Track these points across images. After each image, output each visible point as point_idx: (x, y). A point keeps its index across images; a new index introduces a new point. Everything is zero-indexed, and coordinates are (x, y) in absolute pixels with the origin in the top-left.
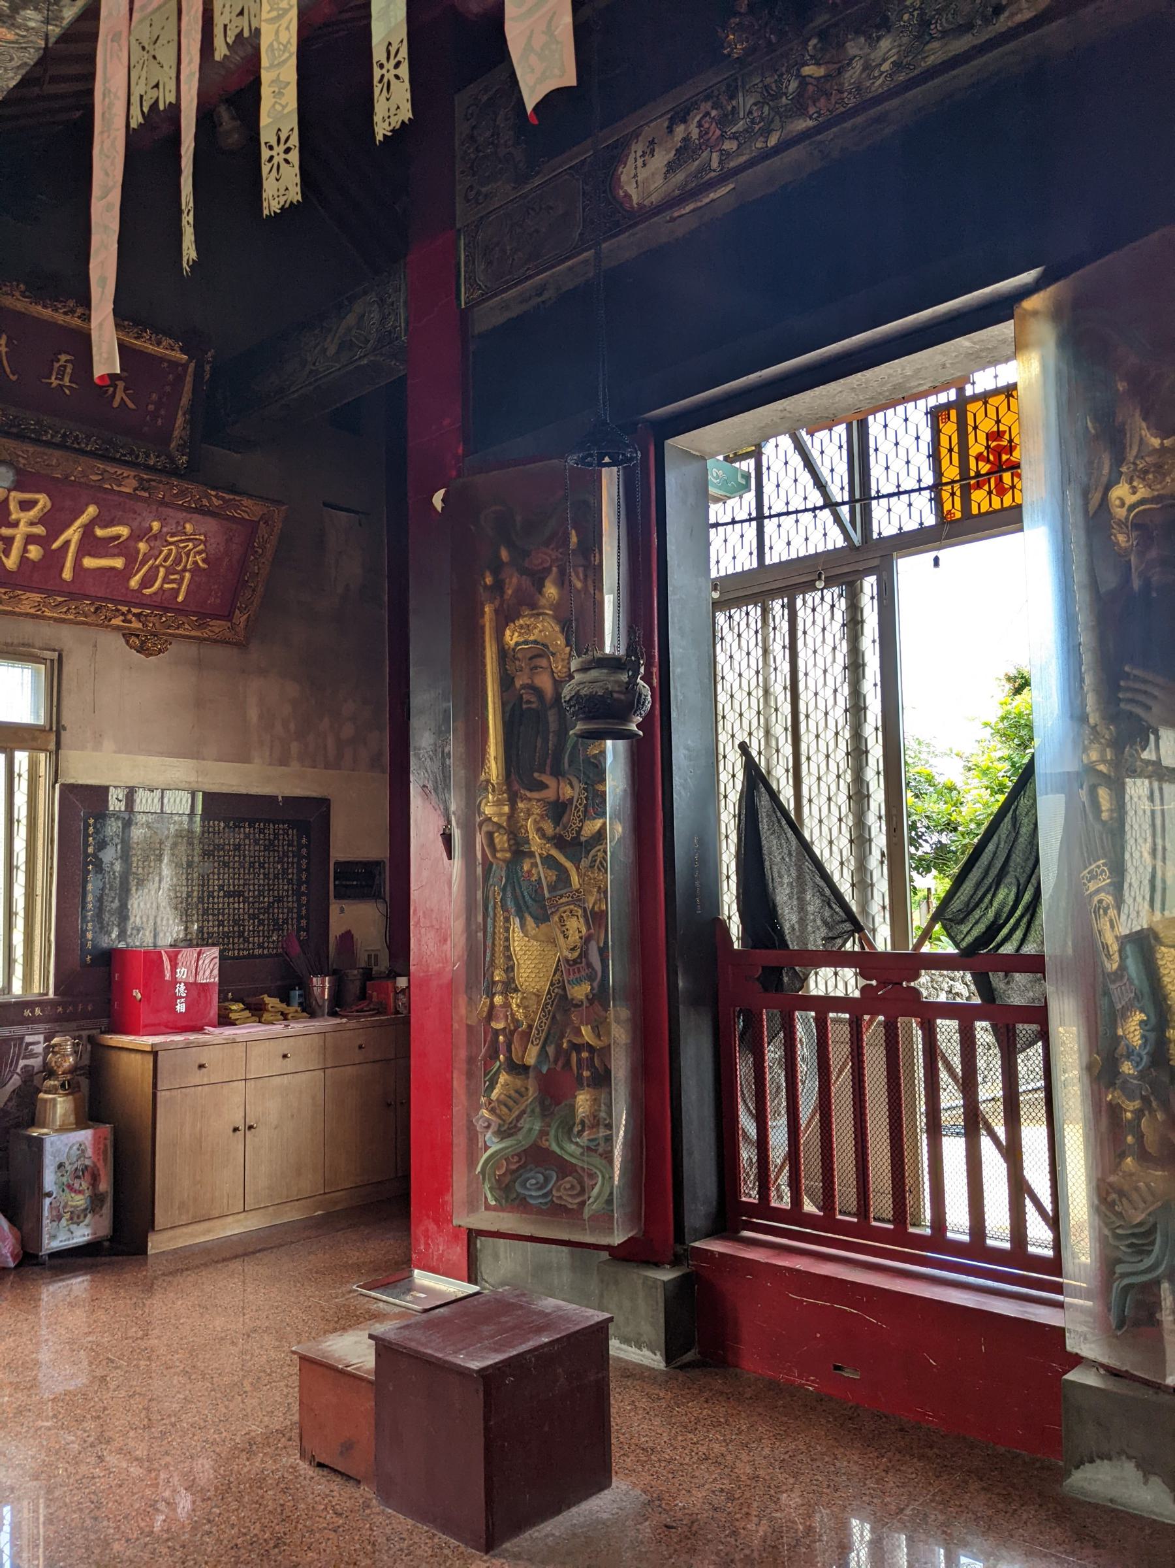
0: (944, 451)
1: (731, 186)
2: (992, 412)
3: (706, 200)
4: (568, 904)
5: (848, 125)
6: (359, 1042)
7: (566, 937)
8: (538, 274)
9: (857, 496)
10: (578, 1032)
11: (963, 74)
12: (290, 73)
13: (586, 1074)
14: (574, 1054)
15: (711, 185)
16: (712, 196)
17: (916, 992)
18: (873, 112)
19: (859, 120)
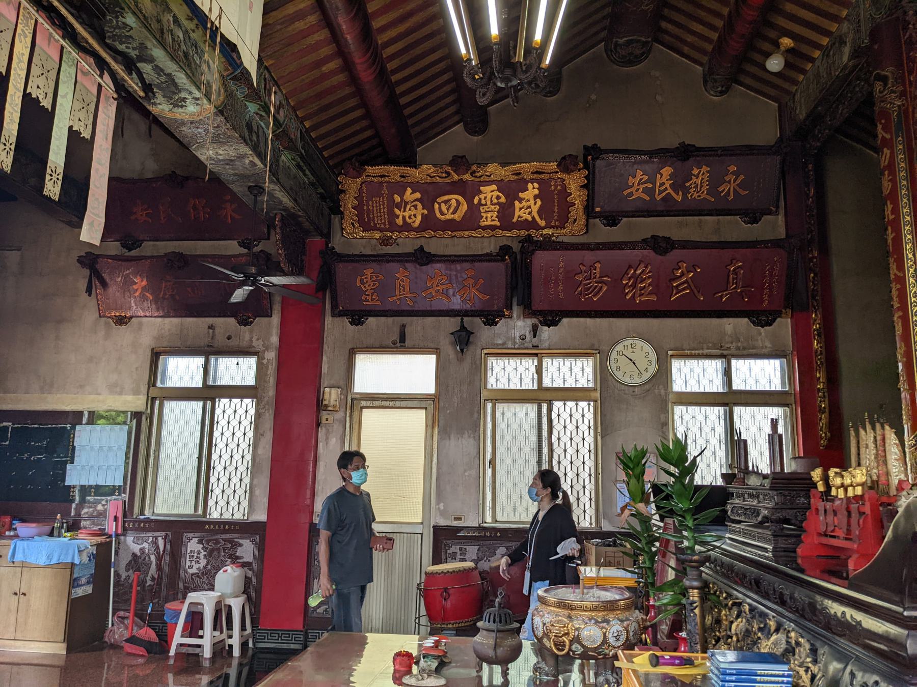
12: (15, 127)
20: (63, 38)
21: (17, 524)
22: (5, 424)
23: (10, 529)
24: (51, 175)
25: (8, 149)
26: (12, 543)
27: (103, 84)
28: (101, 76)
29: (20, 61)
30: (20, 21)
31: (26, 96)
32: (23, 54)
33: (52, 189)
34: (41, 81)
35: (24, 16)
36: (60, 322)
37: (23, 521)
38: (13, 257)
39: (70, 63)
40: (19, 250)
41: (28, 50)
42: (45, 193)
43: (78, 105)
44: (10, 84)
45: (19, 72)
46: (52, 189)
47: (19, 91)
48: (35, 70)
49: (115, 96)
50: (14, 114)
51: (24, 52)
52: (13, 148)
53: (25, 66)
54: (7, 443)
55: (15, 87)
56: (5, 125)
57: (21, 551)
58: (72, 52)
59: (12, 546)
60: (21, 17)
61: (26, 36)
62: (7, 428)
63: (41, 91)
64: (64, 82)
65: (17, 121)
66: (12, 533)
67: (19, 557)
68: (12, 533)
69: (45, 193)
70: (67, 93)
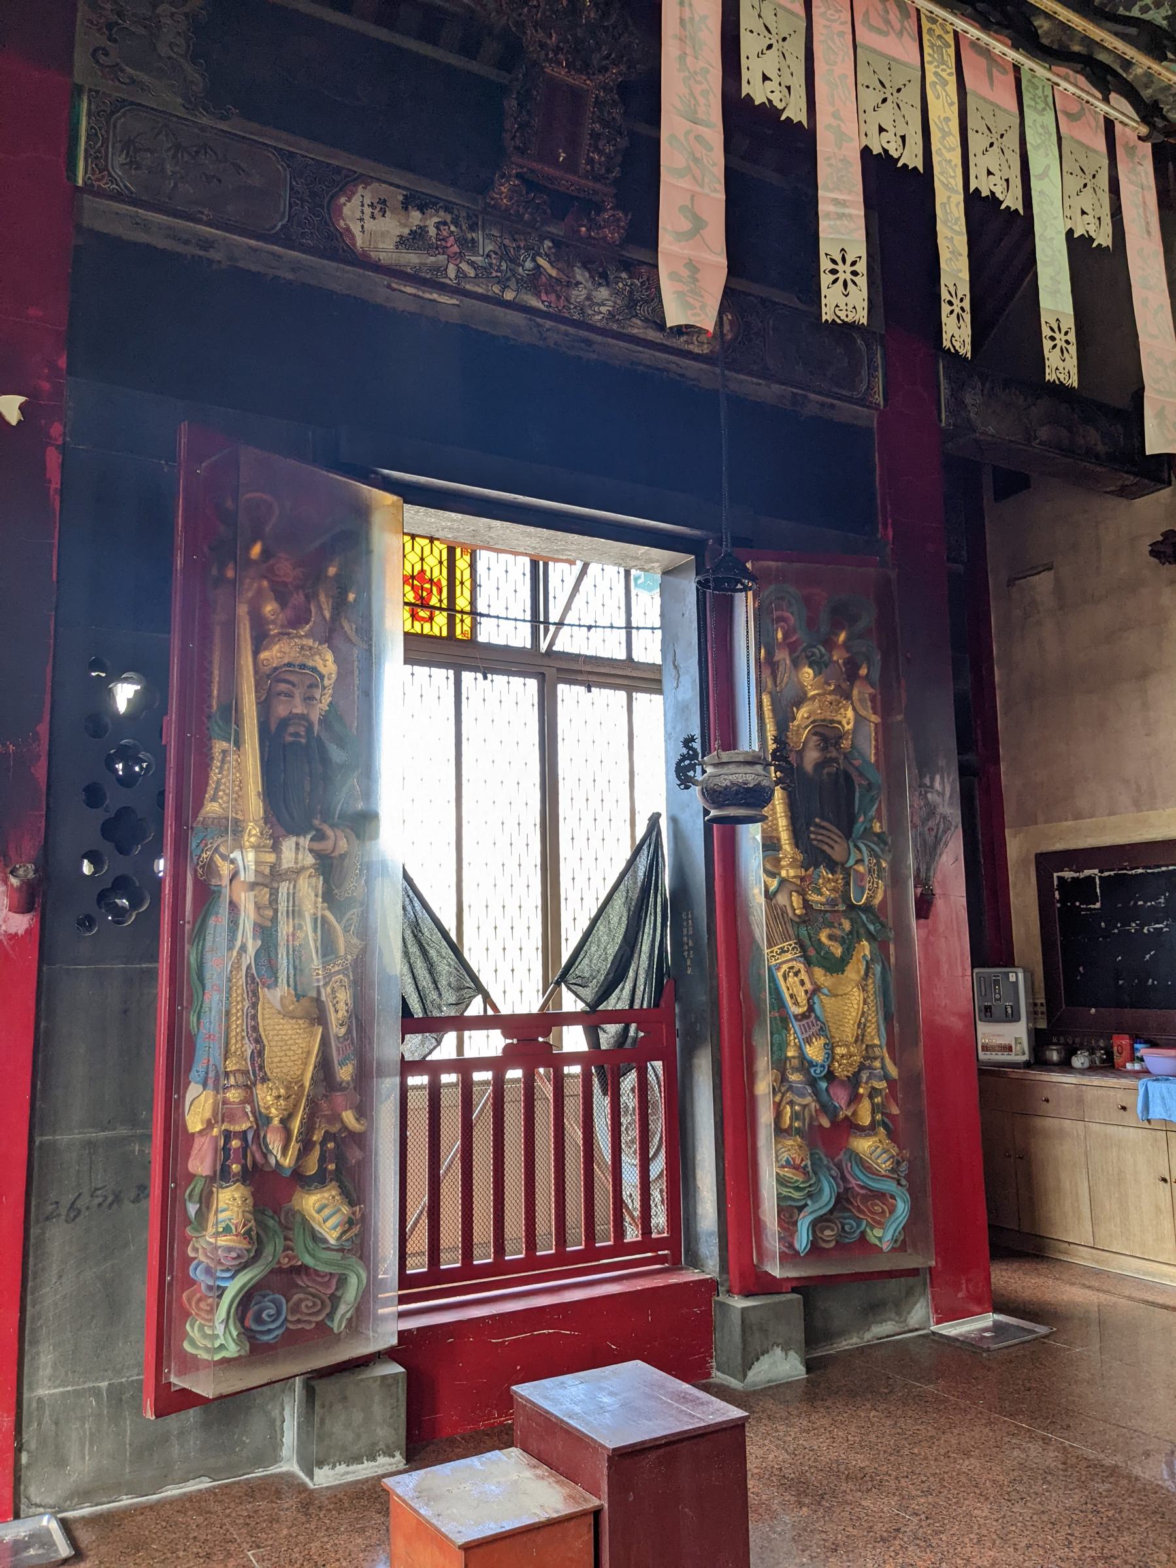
0: (468, 584)
1: (454, 301)
2: (418, 549)
3: (427, 296)
4: (338, 972)
5: (563, 328)
6: (1049, 1105)
7: (337, 1011)
8: (209, 224)
9: (542, 626)
10: (336, 1117)
11: (646, 355)
12: (963, 264)
13: (235, 1168)
14: (788, 1108)
15: (442, 288)
16: (435, 296)
17: (506, 1035)
18: (584, 333)
19: (571, 330)
20: (1015, 47)
21: (1142, 1050)
22: (1087, 872)
23: (1133, 1059)
24: (1053, 339)
25: (957, 310)
26: (1141, 1084)
27: (1114, 114)
28: (1106, 100)
29: (945, 134)
30: (927, 58)
31: (973, 200)
32: (947, 119)
33: (1061, 365)
34: (992, 160)
35: (932, 46)
36: (1144, 675)
37: (1153, 1044)
38: (1043, 583)
39: (1041, 106)
40: (1050, 569)
41: (955, 108)
42: (1050, 376)
43: (1074, 184)
44: (937, 184)
45: (948, 156)
46: (1061, 365)
47: (957, 192)
48: (976, 143)
49: (1144, 130)
50: (956, 238)
51: (948, 114)
52: (967, 307)
53: (955, 140)
54: (1098, 905)
55: (946, 186)
56: (943, 265)
57: (1159, 1101)
58: (1035, 69)
59: (1141, 1091)
60: (927, 50)
61: (945, 83)
62: (1091, 879)
63: (996, 178)
64: (1038, 147)
65: (964, 250)
66: (1137, 1067)
67: (1157, 1112)
68: (1137, 1067)
69: (1050, 376)
70: (1048, 167)
